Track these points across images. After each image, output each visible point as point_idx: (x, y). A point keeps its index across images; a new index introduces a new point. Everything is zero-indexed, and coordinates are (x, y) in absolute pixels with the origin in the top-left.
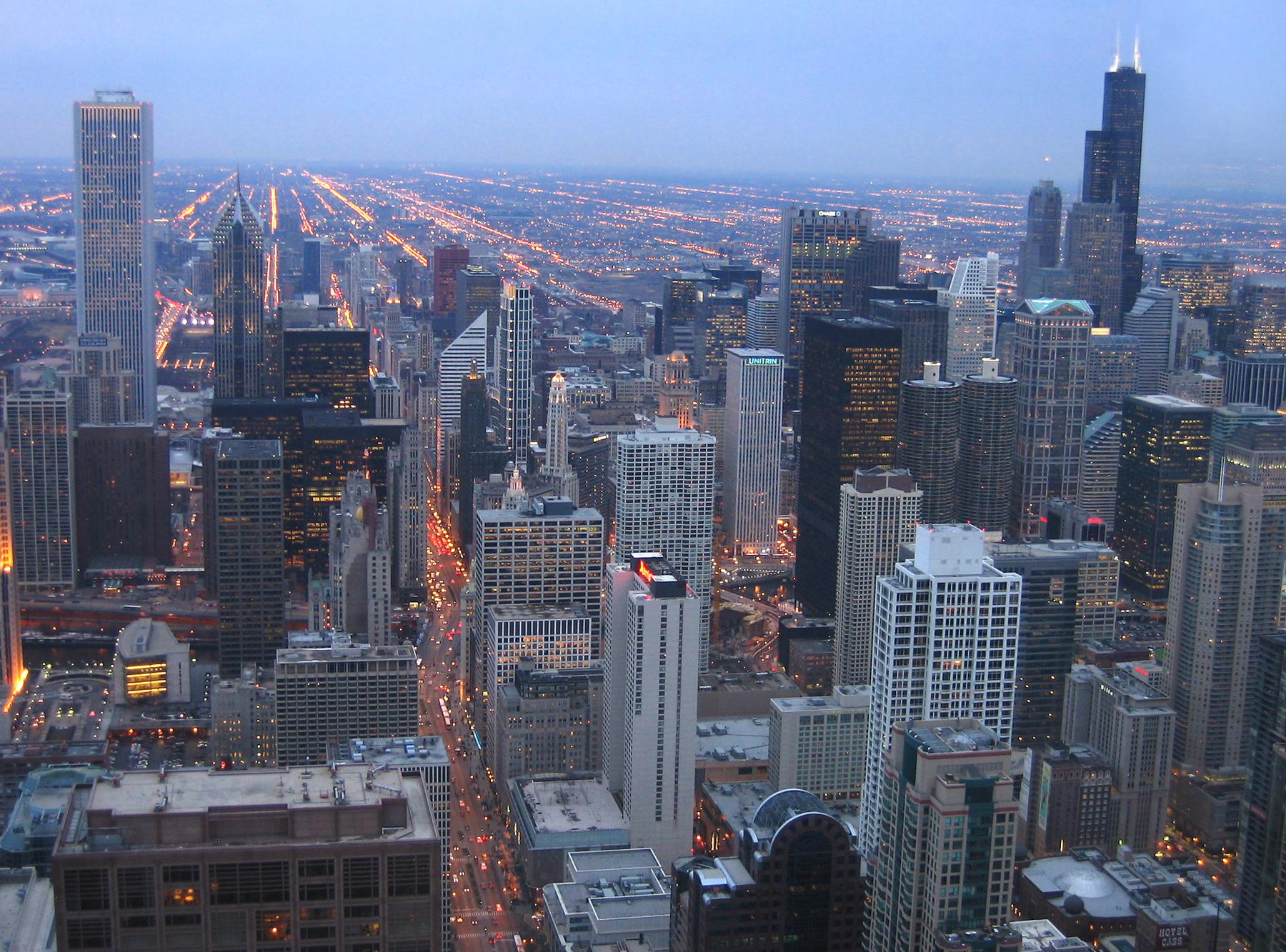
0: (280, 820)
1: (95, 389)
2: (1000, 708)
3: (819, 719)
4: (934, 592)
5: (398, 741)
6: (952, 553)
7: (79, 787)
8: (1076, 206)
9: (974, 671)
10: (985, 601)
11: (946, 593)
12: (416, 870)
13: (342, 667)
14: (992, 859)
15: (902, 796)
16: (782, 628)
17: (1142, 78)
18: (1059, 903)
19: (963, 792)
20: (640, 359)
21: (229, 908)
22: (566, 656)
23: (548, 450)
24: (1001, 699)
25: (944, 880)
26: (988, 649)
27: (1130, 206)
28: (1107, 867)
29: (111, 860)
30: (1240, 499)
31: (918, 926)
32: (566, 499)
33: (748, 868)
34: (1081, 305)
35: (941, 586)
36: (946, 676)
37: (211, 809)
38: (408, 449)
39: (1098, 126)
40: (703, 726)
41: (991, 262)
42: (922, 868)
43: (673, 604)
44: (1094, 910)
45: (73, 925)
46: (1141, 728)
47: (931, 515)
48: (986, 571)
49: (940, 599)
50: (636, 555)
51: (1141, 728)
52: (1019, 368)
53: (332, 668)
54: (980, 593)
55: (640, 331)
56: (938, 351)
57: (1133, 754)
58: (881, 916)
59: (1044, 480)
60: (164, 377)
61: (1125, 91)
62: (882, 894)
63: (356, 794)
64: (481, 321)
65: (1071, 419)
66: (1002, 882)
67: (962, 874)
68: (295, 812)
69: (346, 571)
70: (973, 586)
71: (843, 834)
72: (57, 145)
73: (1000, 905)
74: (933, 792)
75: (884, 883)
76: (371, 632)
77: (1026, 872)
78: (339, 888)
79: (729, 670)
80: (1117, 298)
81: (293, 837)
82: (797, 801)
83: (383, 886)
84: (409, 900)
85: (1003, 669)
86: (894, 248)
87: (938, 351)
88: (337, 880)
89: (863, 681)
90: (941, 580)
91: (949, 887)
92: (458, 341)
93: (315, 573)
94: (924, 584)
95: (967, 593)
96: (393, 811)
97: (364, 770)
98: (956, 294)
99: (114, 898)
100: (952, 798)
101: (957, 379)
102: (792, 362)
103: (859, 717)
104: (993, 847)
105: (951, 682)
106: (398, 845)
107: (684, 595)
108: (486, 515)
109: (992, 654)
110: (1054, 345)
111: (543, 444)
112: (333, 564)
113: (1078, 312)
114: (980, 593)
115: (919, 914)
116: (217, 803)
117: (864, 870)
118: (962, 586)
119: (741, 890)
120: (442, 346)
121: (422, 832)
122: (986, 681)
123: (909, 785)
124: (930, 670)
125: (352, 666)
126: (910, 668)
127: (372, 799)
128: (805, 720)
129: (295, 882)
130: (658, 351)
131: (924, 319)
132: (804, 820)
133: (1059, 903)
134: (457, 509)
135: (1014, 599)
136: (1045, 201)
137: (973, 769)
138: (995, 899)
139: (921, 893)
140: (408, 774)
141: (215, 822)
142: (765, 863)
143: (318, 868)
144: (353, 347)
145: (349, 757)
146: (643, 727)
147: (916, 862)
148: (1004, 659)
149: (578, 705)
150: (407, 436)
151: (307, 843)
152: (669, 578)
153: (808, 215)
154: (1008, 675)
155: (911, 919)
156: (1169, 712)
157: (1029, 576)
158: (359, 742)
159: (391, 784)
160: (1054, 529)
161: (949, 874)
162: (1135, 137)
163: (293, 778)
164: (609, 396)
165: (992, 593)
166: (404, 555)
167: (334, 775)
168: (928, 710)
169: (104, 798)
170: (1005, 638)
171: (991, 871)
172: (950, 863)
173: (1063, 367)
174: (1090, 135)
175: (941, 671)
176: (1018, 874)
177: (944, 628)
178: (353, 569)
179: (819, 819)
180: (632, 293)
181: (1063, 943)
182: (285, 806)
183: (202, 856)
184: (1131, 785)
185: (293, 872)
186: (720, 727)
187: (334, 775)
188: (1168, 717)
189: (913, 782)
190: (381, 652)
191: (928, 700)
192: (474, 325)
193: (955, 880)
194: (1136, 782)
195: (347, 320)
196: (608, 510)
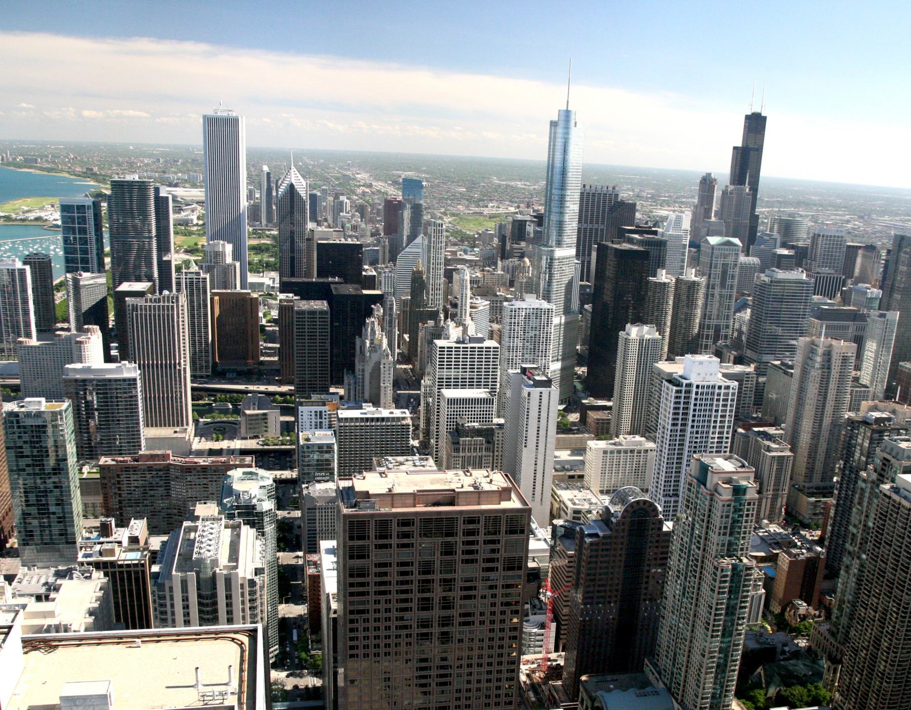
3: (612, 452)
4: (694, 389)
5: (410, 458)
15: (698, 492)
17: (765, 118)
25: (719, 534)
27: (754, 189)
30: (831, 346)
34: (736, 241)
35: (698, 387)
36: (697, 432)
37: (418, 491)
39: (740, 145)
45: (352, 548)
49: (697, 393)
50: (524, 366)
54: (717, 391)
61: (755, 124)
67: (728, 531)
70: (713, 387)
72: (194, 138)
78: (482, 530)
80: (751, 238)
83: (503, 529)
84: (514, 537)
86: (632, 208)
88: (481, 526)
90: (698, 383)
91: (722, 537)
92: (407, 250)
93: (348, 370)
95: (710, 390)
99: (372, 534)
100: (726, 493)
107: (550, 387)
109: (721, 422)
112: (358, 366)
116: (419, 489)
118: (708, 387)
123: (702, 486)
124: (689, 429)
126: (679, 428)
128: (605, 452)
129: (461, 527)
135: (733, 394)
136: (707, 183)
139: (706, 539)
152: (544, 378)
156: (789, 454)
158: (390, 458)
161: (722, 531)
162: (759, 150)
165: (723, 391)
169: (370, 483)
172: (723, 526)
175: (695, 429)
179: (645, 502)
182: (454, 490)
185: (394, 524)
188: (788, 457)
189: (705, 485)
192: (415, 241)
193: (725, 534)
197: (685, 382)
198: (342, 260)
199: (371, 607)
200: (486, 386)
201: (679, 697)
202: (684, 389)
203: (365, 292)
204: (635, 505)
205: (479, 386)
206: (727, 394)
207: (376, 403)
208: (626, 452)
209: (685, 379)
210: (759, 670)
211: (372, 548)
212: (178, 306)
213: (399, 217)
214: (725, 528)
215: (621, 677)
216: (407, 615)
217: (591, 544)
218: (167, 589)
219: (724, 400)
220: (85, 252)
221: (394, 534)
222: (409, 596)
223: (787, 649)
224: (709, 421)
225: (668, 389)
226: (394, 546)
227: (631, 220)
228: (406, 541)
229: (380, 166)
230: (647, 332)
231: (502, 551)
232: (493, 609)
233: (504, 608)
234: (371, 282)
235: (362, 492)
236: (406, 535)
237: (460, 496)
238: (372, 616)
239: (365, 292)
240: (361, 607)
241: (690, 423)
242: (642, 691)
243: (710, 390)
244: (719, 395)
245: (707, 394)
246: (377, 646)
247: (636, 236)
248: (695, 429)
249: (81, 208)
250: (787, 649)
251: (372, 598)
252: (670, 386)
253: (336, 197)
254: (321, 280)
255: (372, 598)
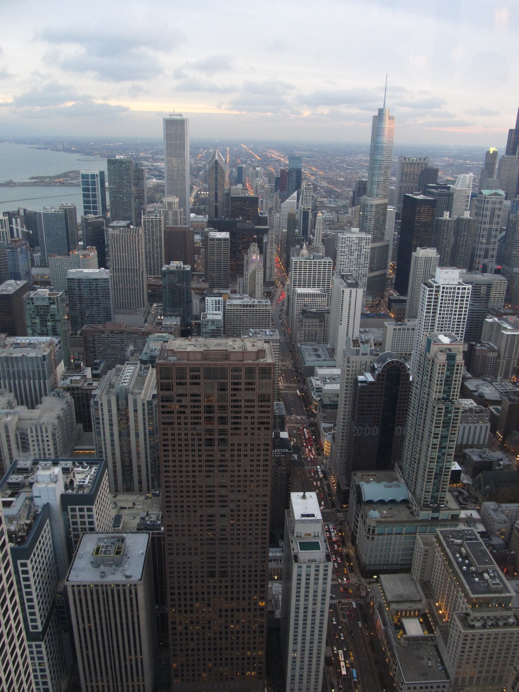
0: (226, 355)
1: (170, 213)
2: (462, 323)
4: (441, 290)
5: (264, 330)
6: (449, 277)
7: (164, 342)
8: (503, 157)
9: (453, 316)
10: (458, 293)
11: (445, 290)
12: (267, 371)
13: (247, 306)
14: (454, 379)
16: (389, 299)
18: (476, 394)
19: (446, 356)
20: (347, 208)
21: (209, 381)
22: (236, 474)
23: (315, 238)
24: (462, 323)
25: (437, 384)
26: (458, 309)
28: (493, 383)
29: (174, 364)
31: (428, 399)
32: (320, 254)
33: (373, 376)
35: (443, 288)
36: (443, 318)
38: (270, 236)
39: (514, 127)
40: (361, 330)
41: (470, 177)
42: (430, 380)
43: (354, 290)
44: (487, 397)
45: (162, 384)
46: (510, 339)
47: (442, 264)
48: (459, 284)
49: (443, 292)
51: (510, 339)
52: (477, 214)
53: (244, 306)
54: (457, 291)
55: (348, 198)
56: (449, 208)
57: (505, 350)
58: (416, 394)
59: (482, 253)
60: (192, 211)
62: (417, 387)
63: (249, 347)
64: (295, 194)
65: (493, 233)
66: (457, 386)
67: (443, 383)
68: (230, 352)
69: (249, 276)
70: (455, 288)
71: (405, 367)
72: (158, 133)
73: (459, 371)
74: (436, 356)
75: (417, 383)
76: (256, 295)
77: (465, 383)
79: (371, 315)
81: (230, 360)
82: (390, 355)
85: (463, 316)
86: (436, 171)
87: (449, 208)
89: (416, 317)
92: (287, 201)
94: (438, 287)
95: (452, 290)
96: (261, 353)
97: (252, 340)
98: (457, 187)
99: (174, 376)
100: (442, 358)
101: (455, 217)
102: (399, 210)
103: (413, 329)
104: (455, 375)
105: (444, 320)
106: (262, 364)
108: (294, 259)
109: (459, 311)
110: (490, 206)
111: (314, 236)
112: (245, 273)
113: (499, 195)
114: (457, 291)
115: (428, 394)
117: (411, 379)
118: (451, 288)
119: (371, 383)
120: (282, 202)
121: (269, 360)
122: (456, 320)
124: (438, 316)
125: (250, 306)
126: (431, 314)
127: (255, 349)
129: (230, 374)
130: (353, 205)
131: (446, 198)
132: (393, 362)
133: (476, 394)
134: (285, 256)
135: (468, 293)
136: (490, 158)
137: (450, 350)
138: (454, 392)
140: (267, 342)
141: (205, 355)
142: (379, 375)
143: (236, 370)
144: (254, 201)
145: (248, 335)
146: (342, 329)
147: (429, 378)
148: (463, 313)
149: (321, 321)
150: (270, 232)
151: (233, 362)
153: (407, 159)
154: (464, 318)
155: (425, 396)
157: (474, 285)
158: (252, 330)
159: (260, 345)
160: (484, 270)
161: (439, 383)
163: (230, 342)
164: (336, 220)
166: (268, 271)
167: (243, 341)
168: (436, 328)
170: (464, 306)
171: (453, 382)
173: (489, 234)
174: (511, 131)
175: (442, 316)
176: (462, 384)
177: (443, 302)
178: (251, 275)
180: (347, 183)
181: (476, 407)
183: (202, 364)
184: (504, 357)
185: (229, 370)
186: (367, 330)
187: (243, 341)
189: (429, 352)
190: (259, 302)
191: (436, 325)
194: (506, 356)
195: (251, 194)
196: (334, 258)
197: (435, 285)
198: (247, 206)
199: (176, 421)
200: (319, 286)
201: (412, 490)
202: (434, 289)
203: (256, 227)
204: (387, 366)
205: (314, 286)
206: (464, 293)
207: (252, 295)
208: (408, 329)
209: (436, 283)
210: (479, 476)
211: (175, 384)
212: (138, 235)
213: (288, 180)
214: (441, 381)
215: (378, 474)
216: (198, 427)
217: (362, 387)
218: (99, 405)
219: (461, 297)
220: (95, 202)
221: (188, 377)
222: (199, 415)
223: (501, 463)
224: (451, 311)
225: (424, 289)
226: (188, 383)
227: (435, 181)
228: (195, 381)
229: (280, 148)
230: (431, 253)
231: (257, 390)
232: (253, 426)
233: (260, 426)
234: (263, 221)
235: (171, 350)
236: (196, 377)
237: (231, 354)
238: (176, 426)
239: (256, 227)
240: (169, 421)
241: (438, 312)
242: (389, 484)
243: (452, 290)
244: (458, 293)
245: (450, 293)
246: (180, 445)
247: (434, 190)
248: (442, 316)
249: (93, 176)
250: (501, 463)
251: (176, 415)
252: (426, 287)
253: (254, 168)
254: (233, 220)
255: (176, 415)
